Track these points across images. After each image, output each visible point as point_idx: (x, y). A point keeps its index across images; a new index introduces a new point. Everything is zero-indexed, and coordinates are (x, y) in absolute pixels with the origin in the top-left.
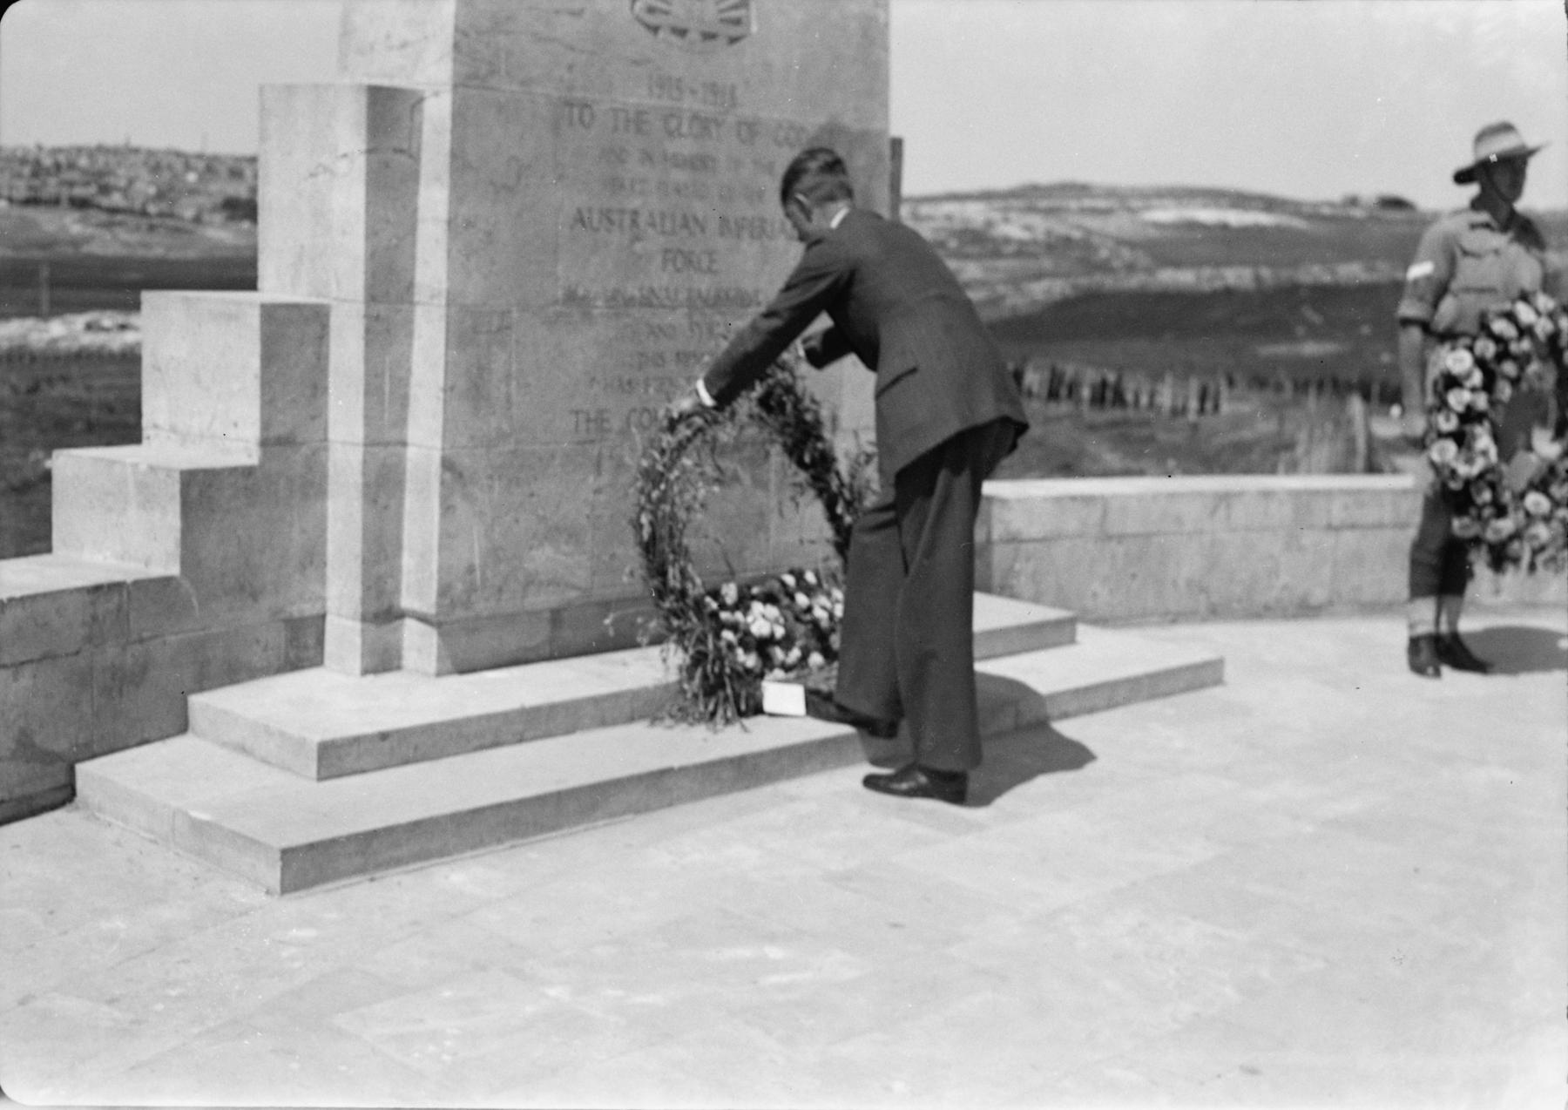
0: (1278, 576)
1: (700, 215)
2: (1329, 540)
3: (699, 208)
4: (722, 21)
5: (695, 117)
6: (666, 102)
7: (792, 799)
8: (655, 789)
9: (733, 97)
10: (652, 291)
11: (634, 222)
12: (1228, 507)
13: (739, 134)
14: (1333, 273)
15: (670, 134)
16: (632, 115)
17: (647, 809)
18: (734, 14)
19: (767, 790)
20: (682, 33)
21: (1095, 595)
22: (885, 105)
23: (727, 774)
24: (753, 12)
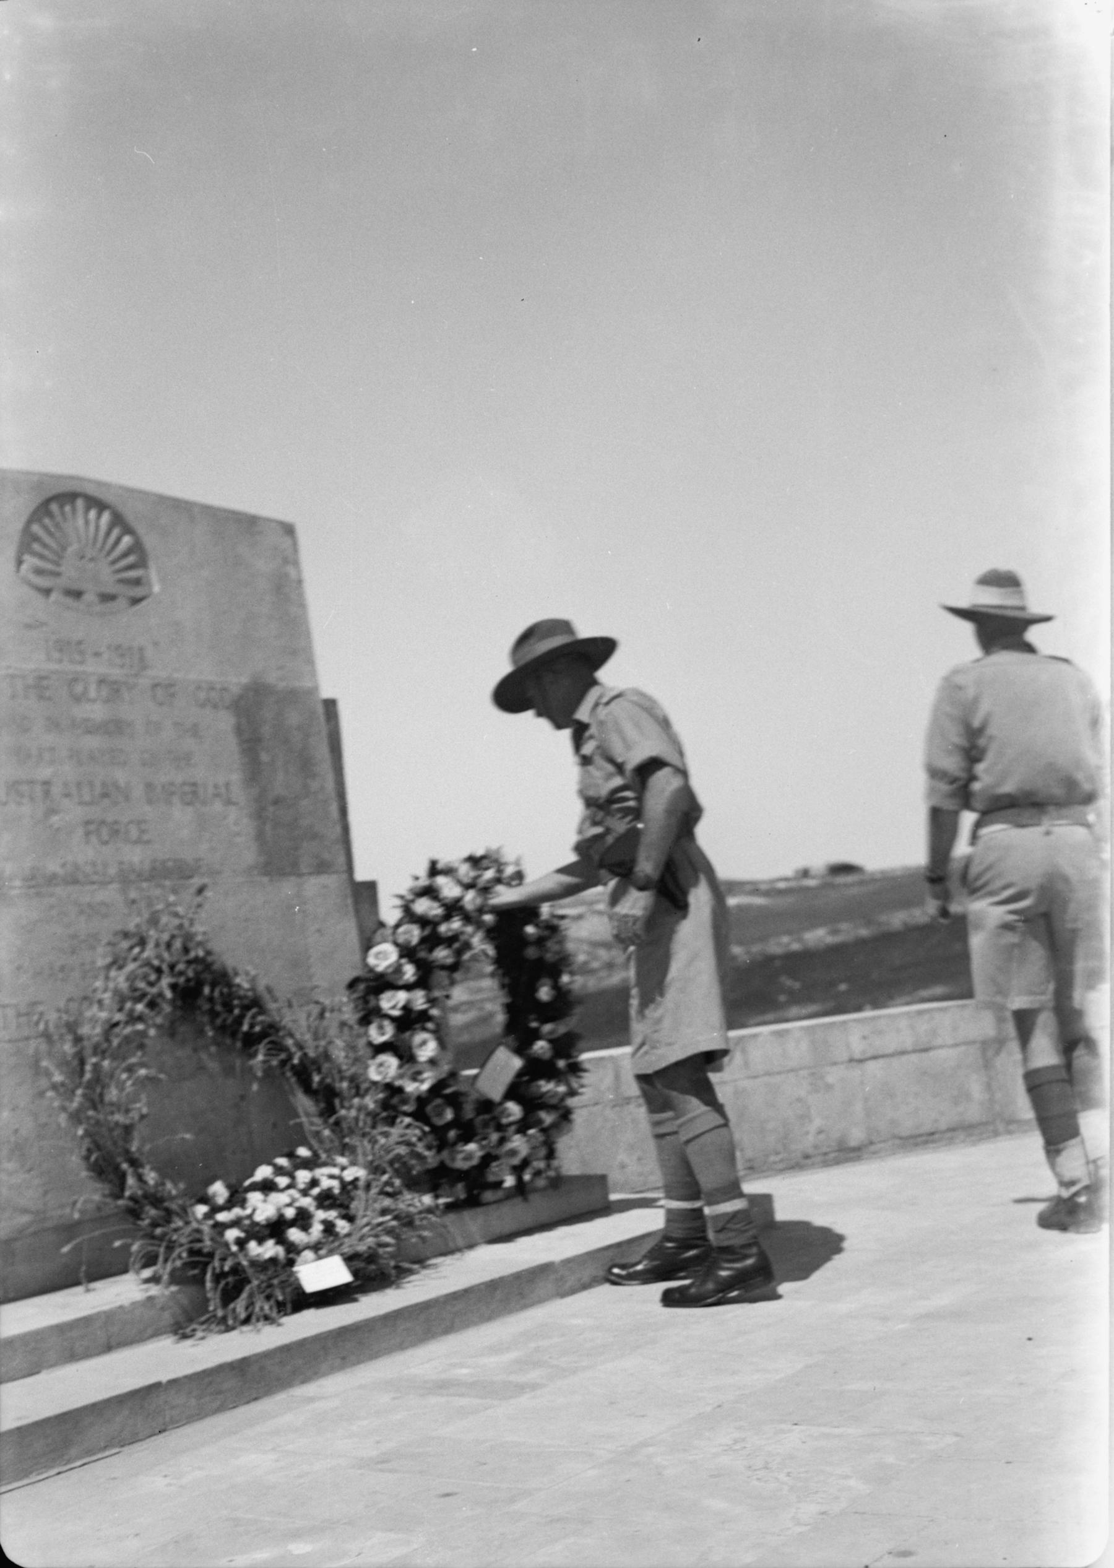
0: (811, 1121)
1: (122, 783)
2: (856, 1073)
3: (121, 776)
4: (122, 581)
5: (102, 681)
6: (67, 667)
7: (311, 1400)
8: (143, 1414)
9: (142, 659)
10: (77, 867)
11: (47, 793)
12: (744, 1051)
13: (154, 697)
14: (800, 940)
15: (78, 699)
16: (30, 681)
17: (135, 1439)
18: (133, 574)
19: (281, 1397)
20: (77, 594)
21: (623, 1166)
22: (310, 661)
23: (230, 1383)
24: (153, 575)
